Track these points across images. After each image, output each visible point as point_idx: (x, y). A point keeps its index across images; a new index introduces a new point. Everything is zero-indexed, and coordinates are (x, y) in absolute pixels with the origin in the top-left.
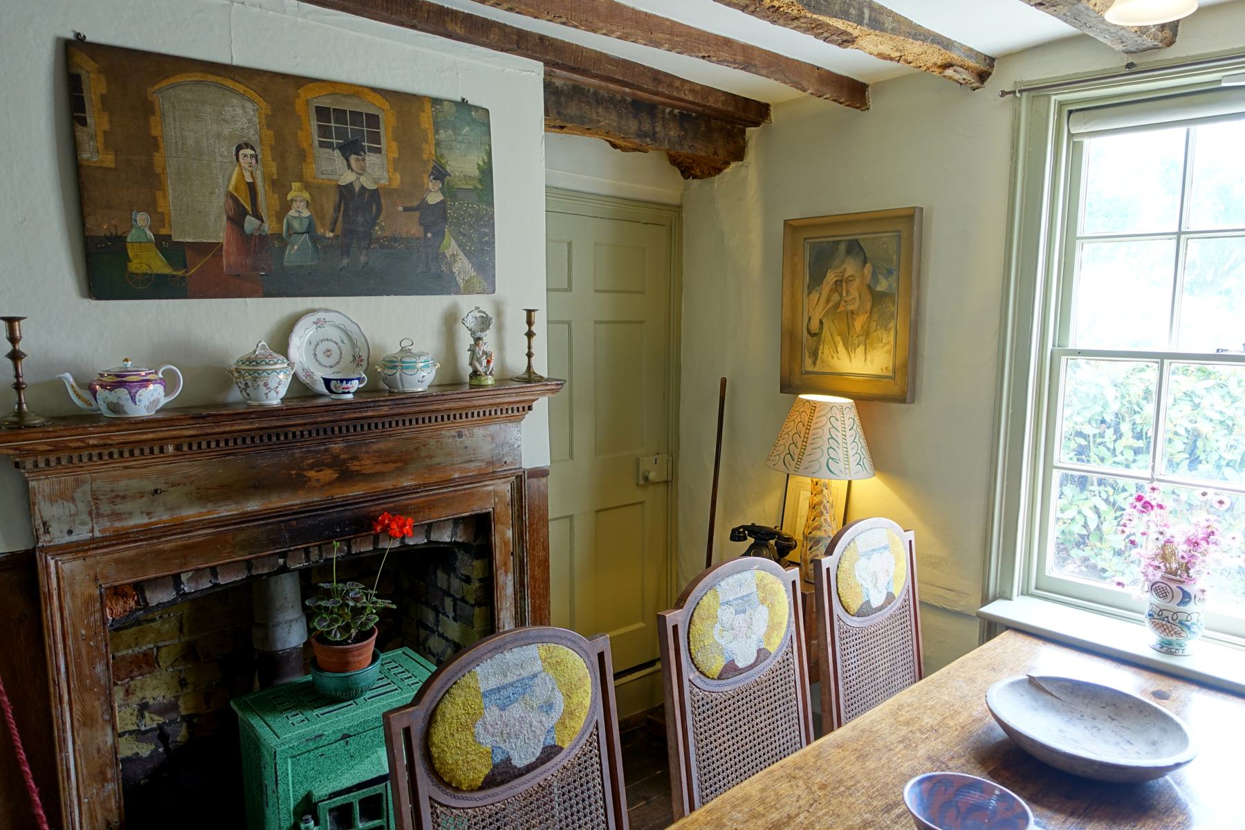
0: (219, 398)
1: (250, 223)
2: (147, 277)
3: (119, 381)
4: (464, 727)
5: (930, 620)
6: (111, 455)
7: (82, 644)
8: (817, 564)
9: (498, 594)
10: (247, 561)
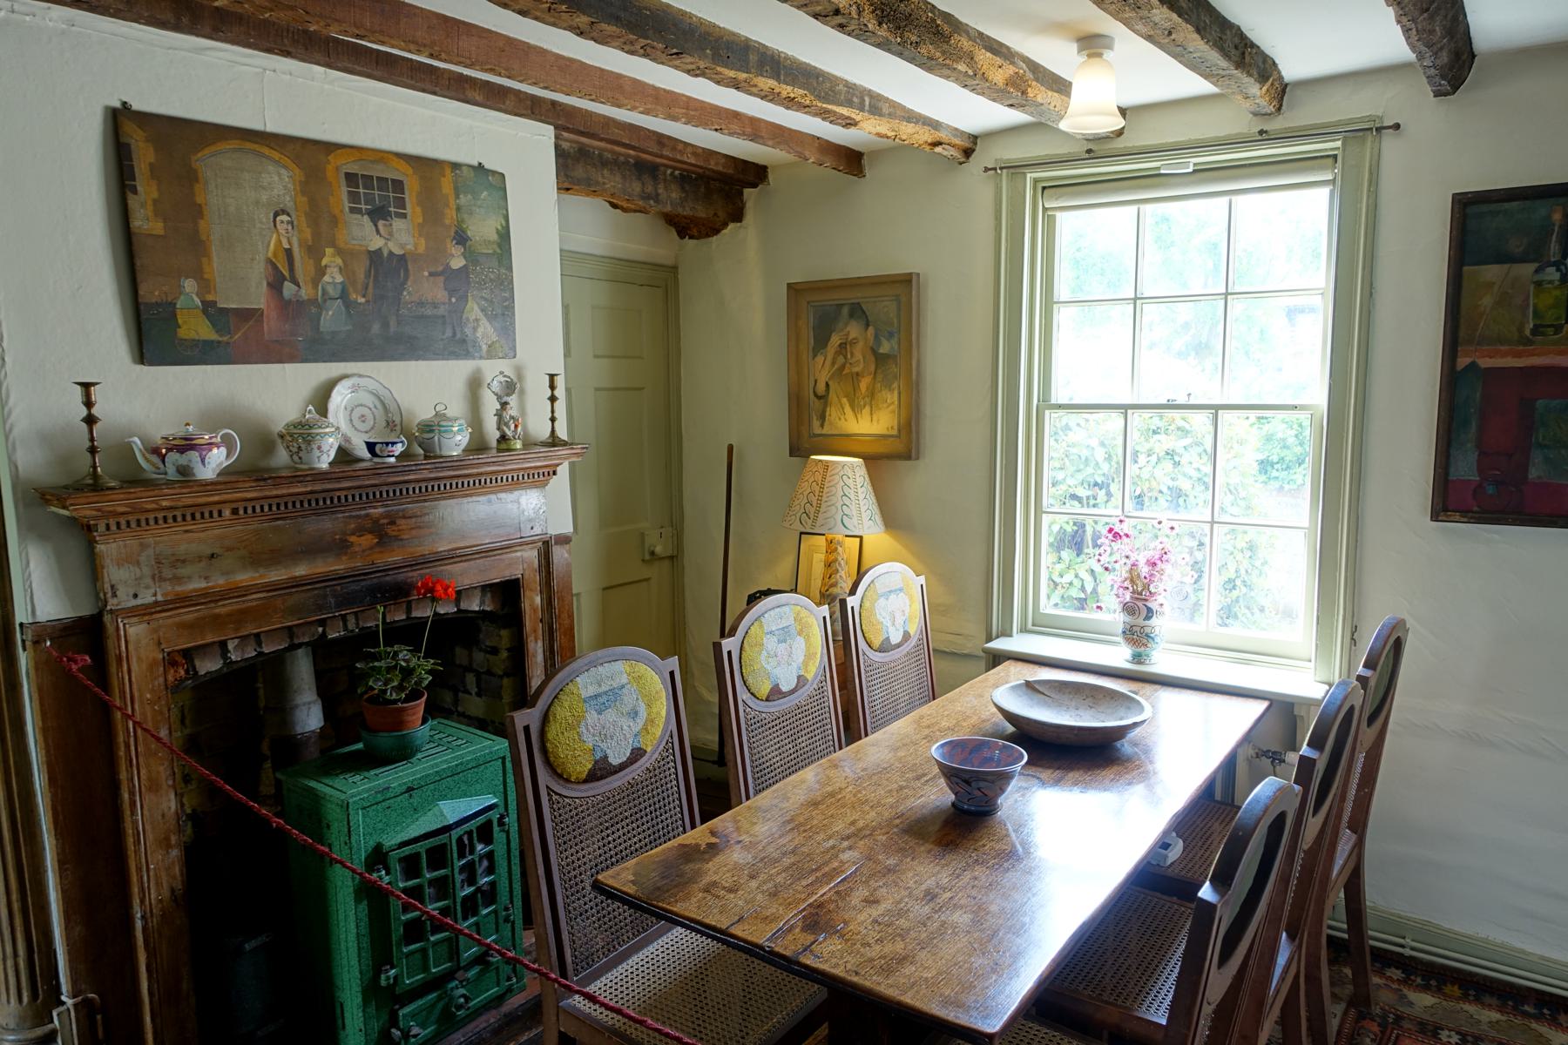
0: (263, 464)
1: (288, 289)
2: (195, 343)
3: (186, 445)
4: (571, 727)
5: (940, 665)
6: (175, 518)
7: (148, 708)
8: (843, 603)
9: (529, 662)
10: (289, 628)
